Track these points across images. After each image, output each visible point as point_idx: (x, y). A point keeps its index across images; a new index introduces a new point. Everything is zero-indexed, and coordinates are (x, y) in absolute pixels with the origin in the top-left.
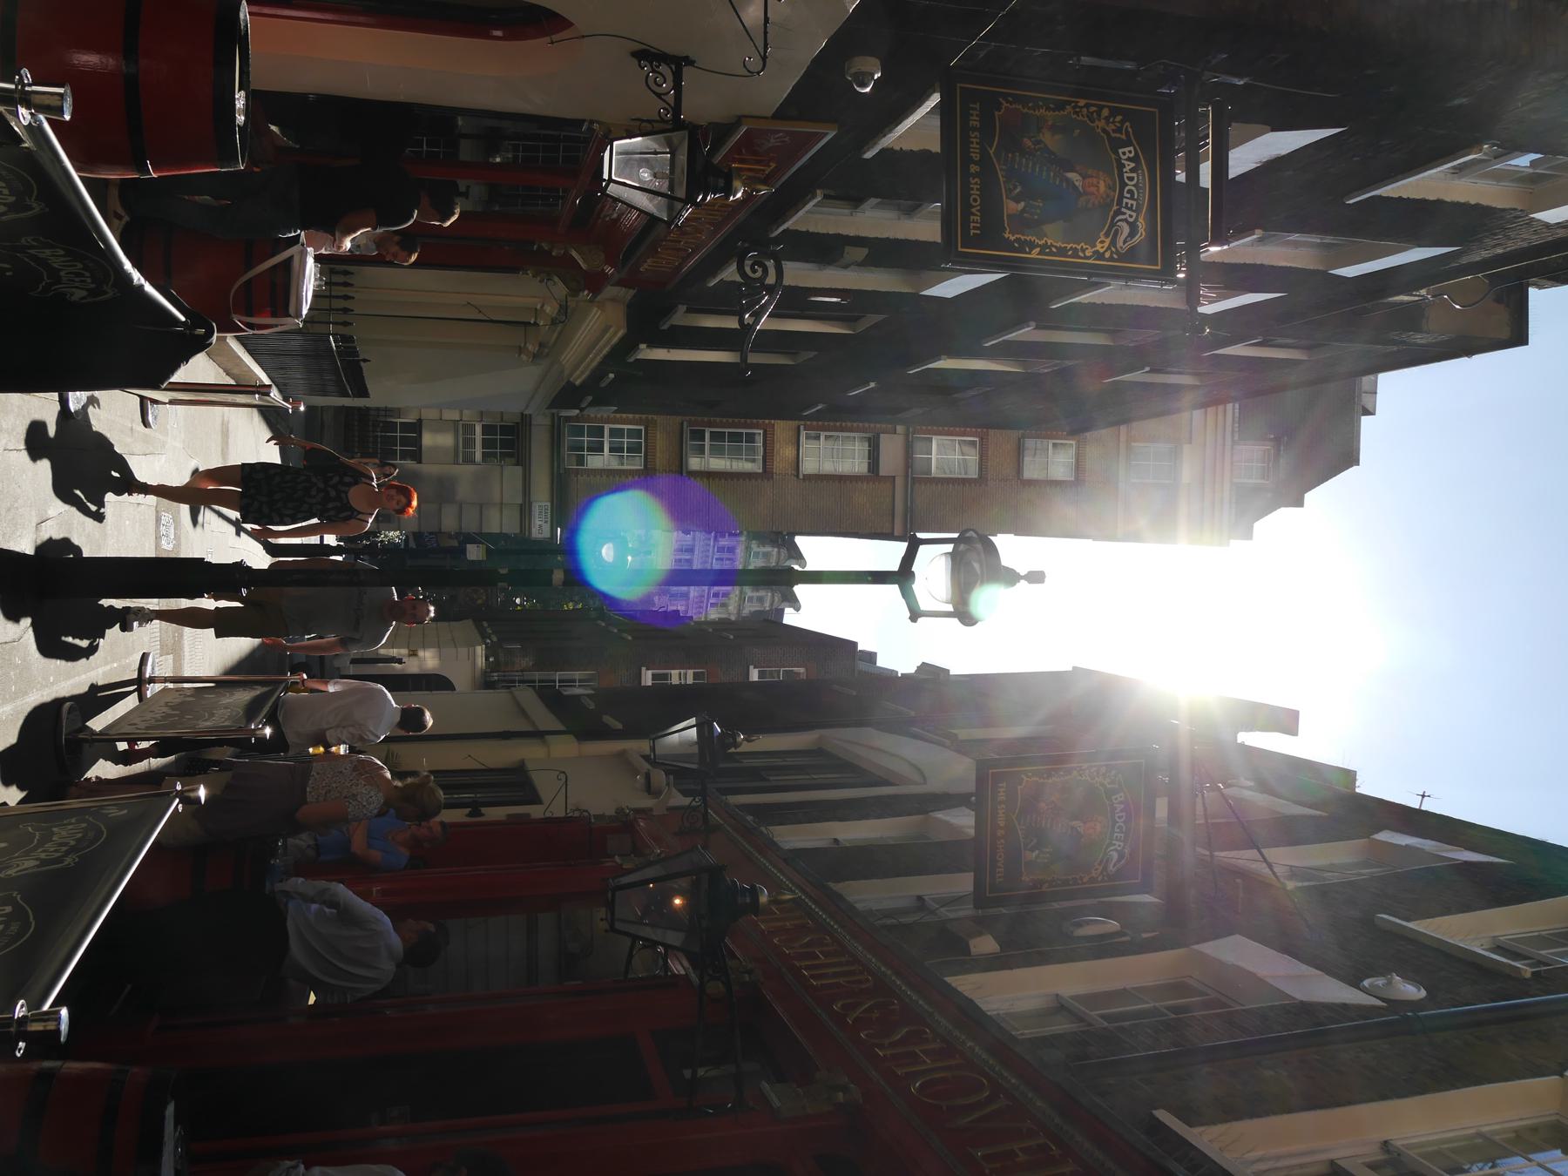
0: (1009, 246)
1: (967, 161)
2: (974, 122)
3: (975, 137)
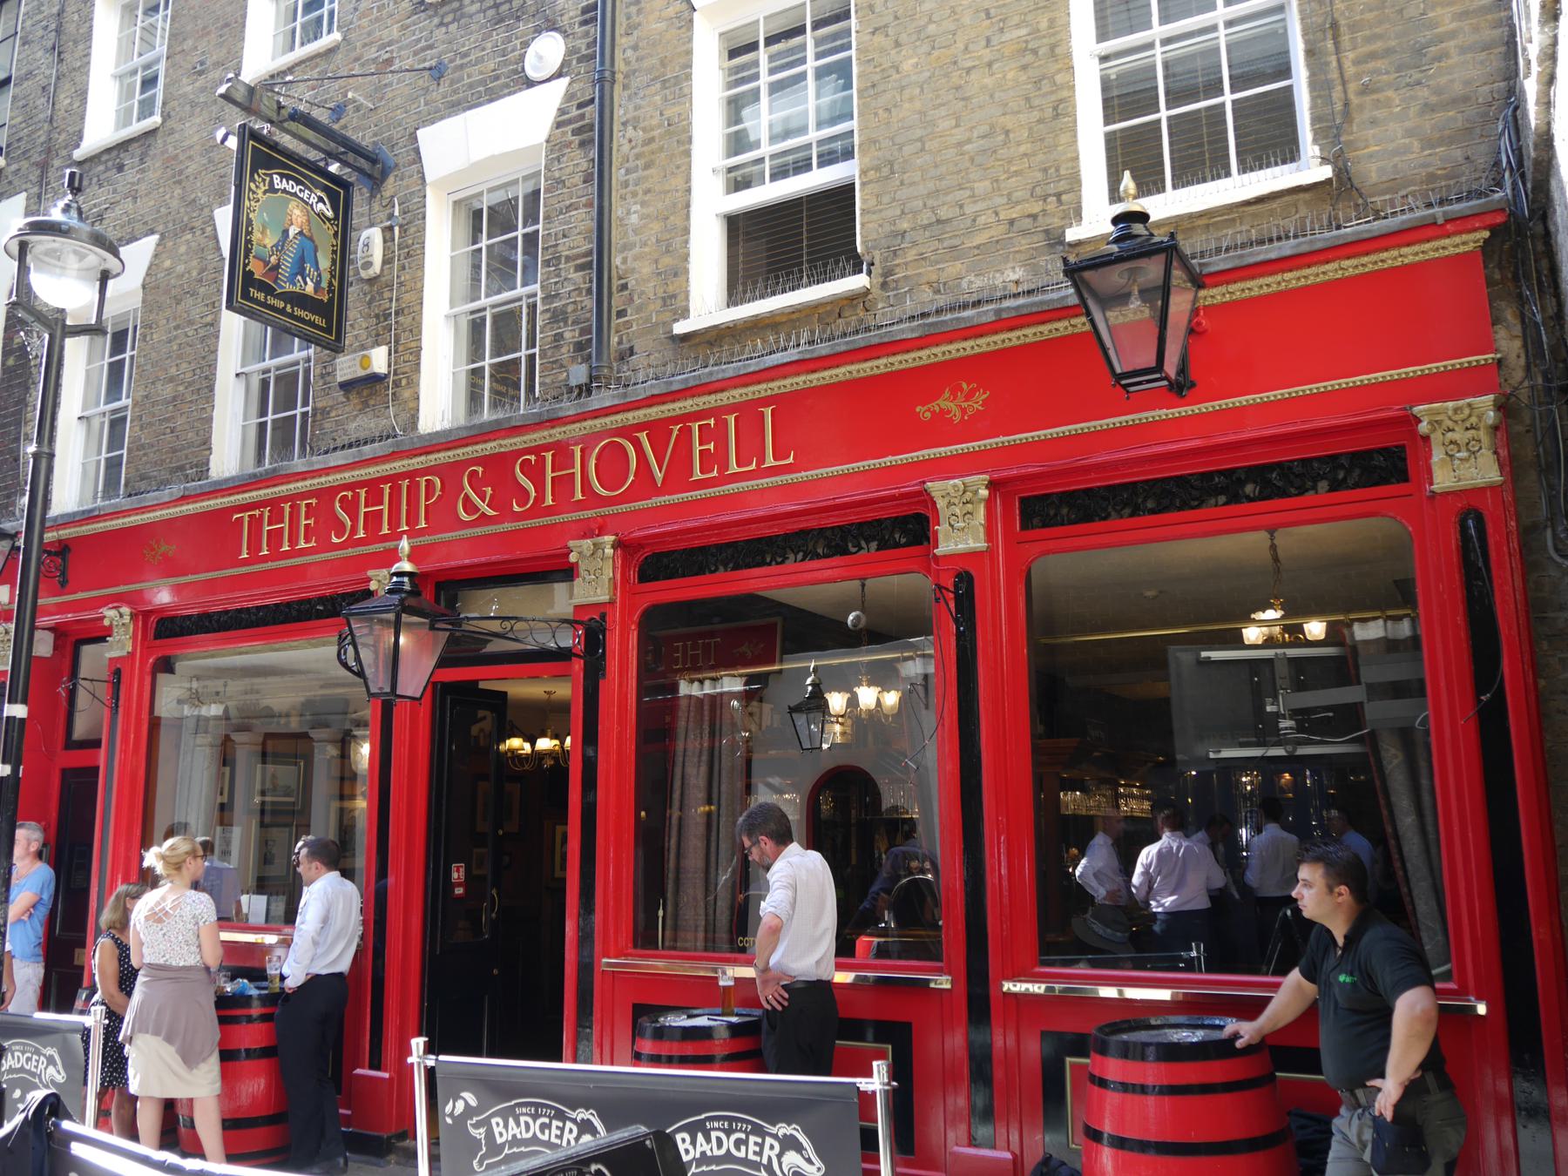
0: (331, 300)
1: (282, 312)
2: (261, 296)
3: (271, 301)
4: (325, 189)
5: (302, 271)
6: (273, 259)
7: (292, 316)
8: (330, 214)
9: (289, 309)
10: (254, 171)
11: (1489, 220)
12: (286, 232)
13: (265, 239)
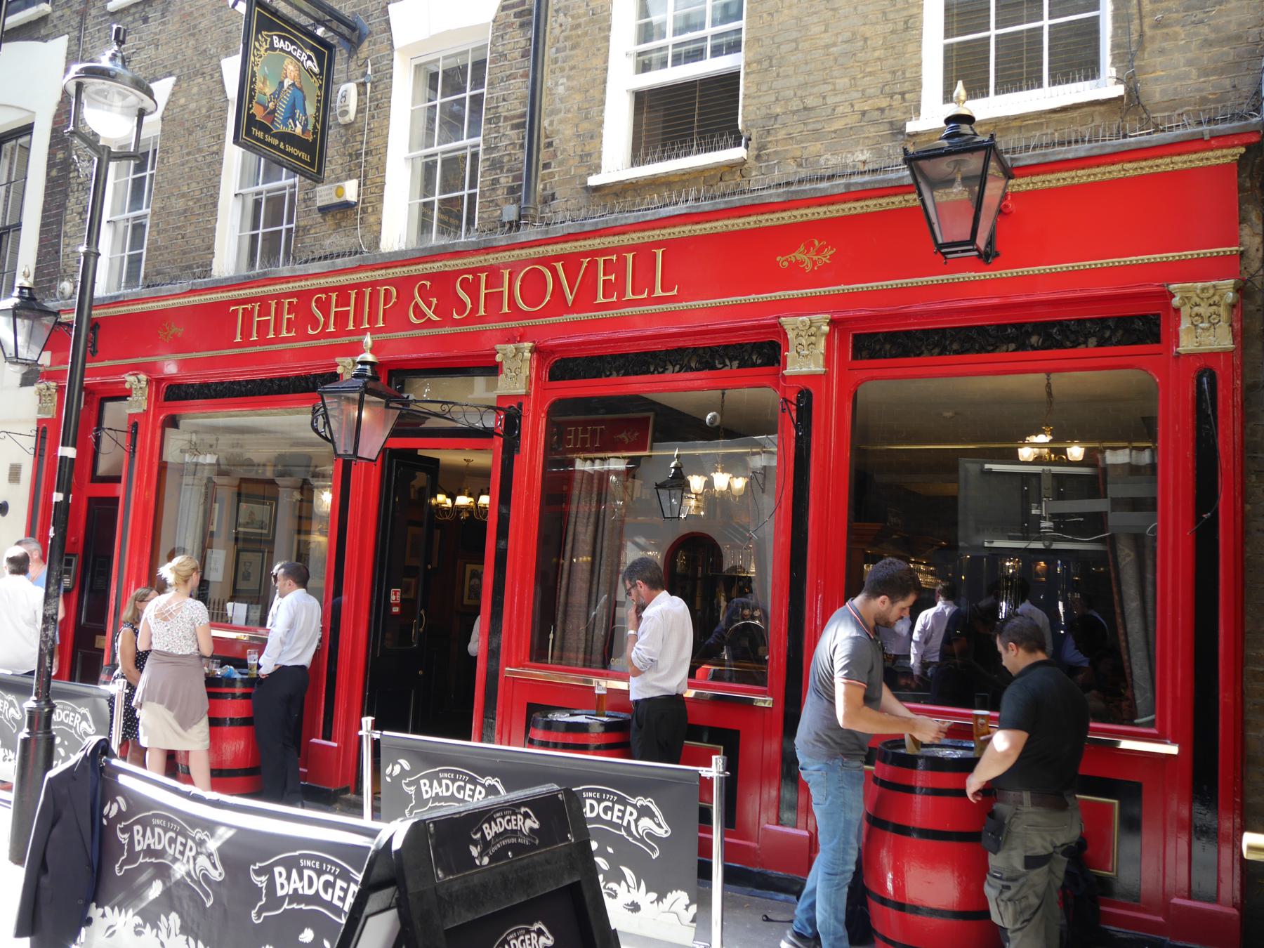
0: (315, 140)
2: (260, 134)
3: (268, 139)
4: (313, 49)
5: (293, 116)
6: (271, 105)
7: (283, 152)
8: (316, 70)
9: (282, 146)
10: (258, 32)
11: (1246, 139)
12: (281, 83)
13: (266, 89)
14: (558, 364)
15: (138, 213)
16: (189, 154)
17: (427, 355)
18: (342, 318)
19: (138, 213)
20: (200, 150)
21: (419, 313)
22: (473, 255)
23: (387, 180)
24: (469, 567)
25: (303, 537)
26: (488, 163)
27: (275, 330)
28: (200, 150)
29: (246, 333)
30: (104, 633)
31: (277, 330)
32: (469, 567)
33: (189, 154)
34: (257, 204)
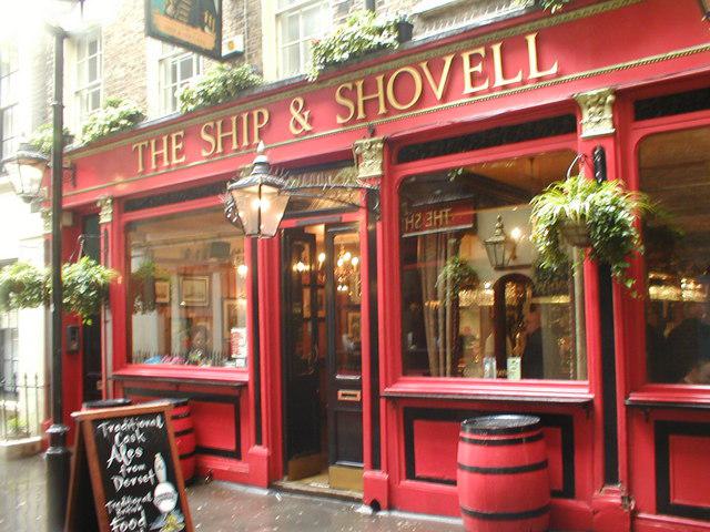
14: (400, 150)
15: (94, 83)
16: (124, 35)
17: (687, 503)
18: (227, 141)
19: (94, 83)
20: (131, 32)
21: (297, 125)
22: (164, 216)
23: (264, 61)
24: (351, 315)
25: (232, 302)
26: (337, 8)
27: (143, 165)
28: (131, 32)
29: (146, 163)
30: (100, 379)
31: (169, 159)
32: (351, 315)
33: (124, 35)
34: (174, 67)
